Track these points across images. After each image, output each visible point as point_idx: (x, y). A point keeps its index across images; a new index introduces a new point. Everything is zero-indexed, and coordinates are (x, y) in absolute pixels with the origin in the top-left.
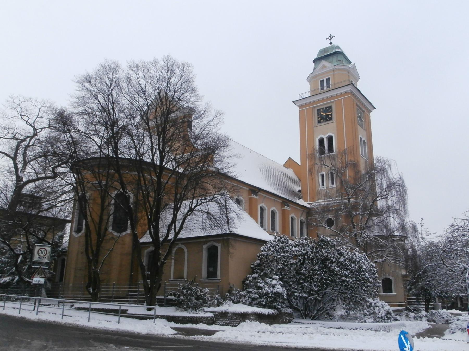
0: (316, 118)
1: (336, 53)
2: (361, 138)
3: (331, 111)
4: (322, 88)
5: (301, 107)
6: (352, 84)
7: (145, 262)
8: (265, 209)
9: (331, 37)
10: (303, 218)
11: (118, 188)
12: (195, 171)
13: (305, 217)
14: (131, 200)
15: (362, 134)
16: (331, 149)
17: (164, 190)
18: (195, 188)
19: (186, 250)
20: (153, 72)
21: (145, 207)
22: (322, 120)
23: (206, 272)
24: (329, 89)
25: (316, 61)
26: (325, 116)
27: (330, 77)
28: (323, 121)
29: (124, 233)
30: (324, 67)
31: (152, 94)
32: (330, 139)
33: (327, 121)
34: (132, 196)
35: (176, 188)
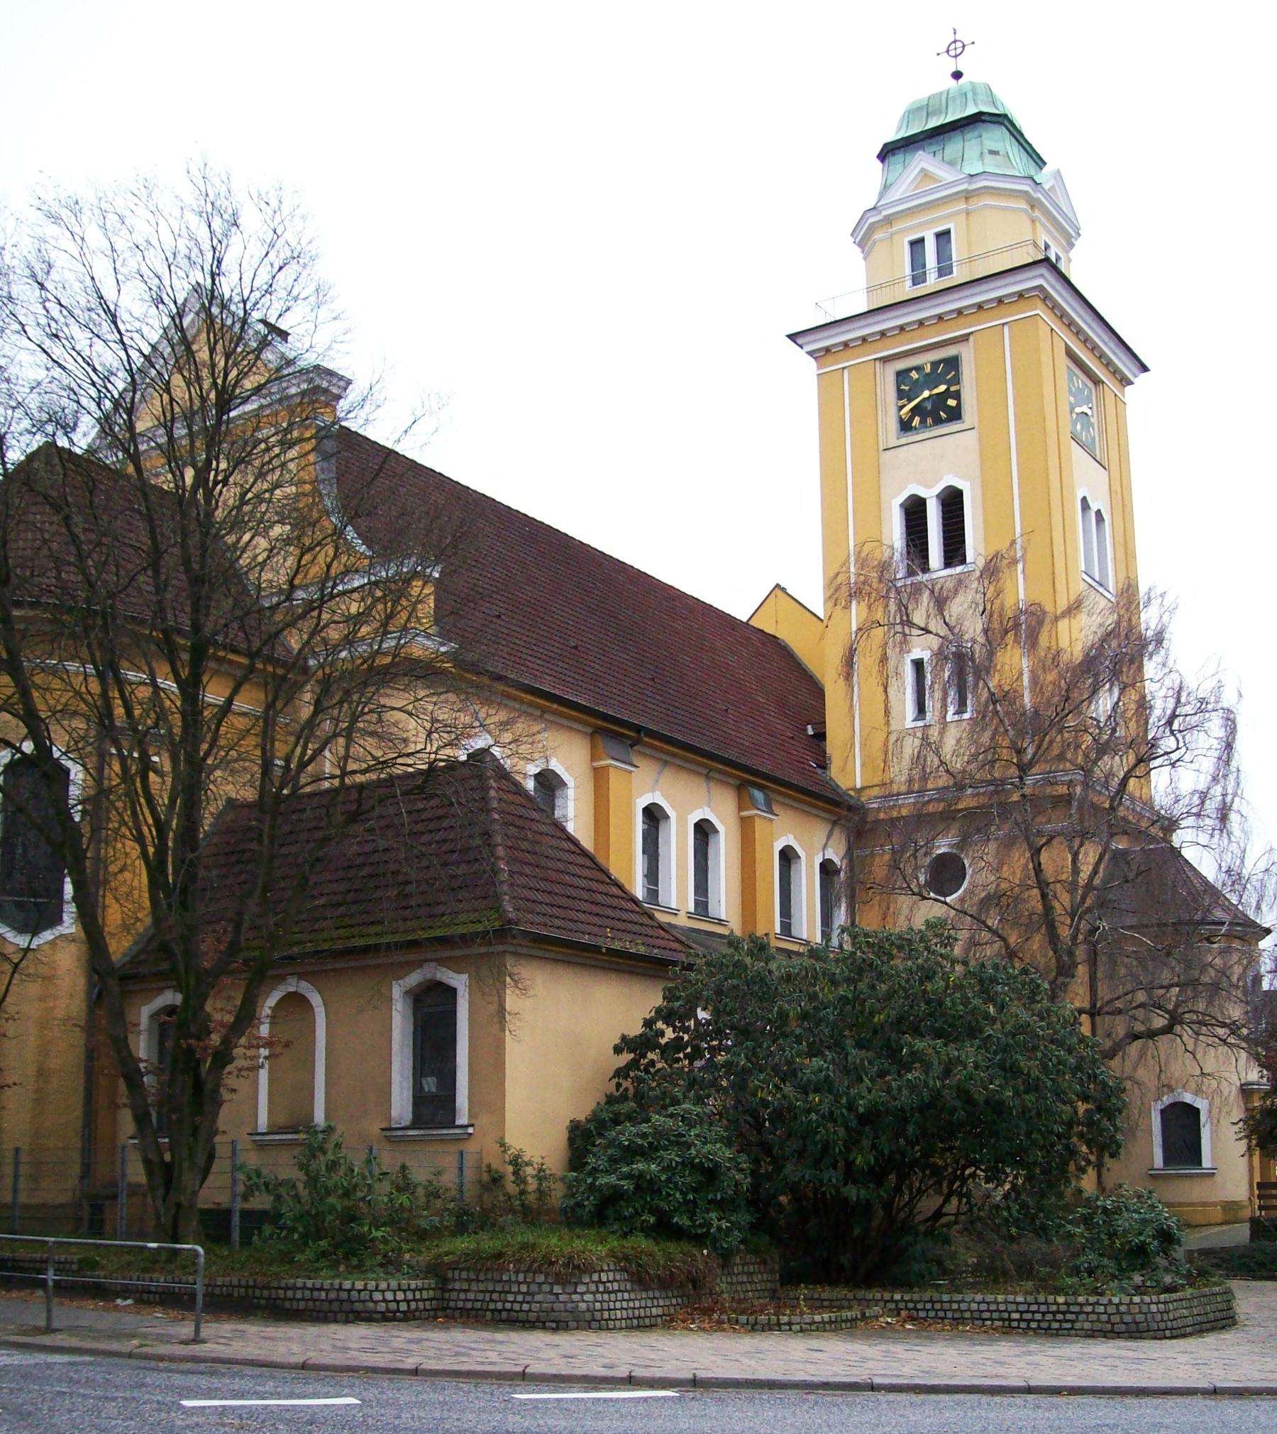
0: (892, 410)
1: (977, 119)
2: (1084, 500)
3: (957, 380)
4: (918, 279)
5: (821, 355)
6: (1047, 260)
7: (143, 1047)
8: (667, 817)
9: (956, 48)
10: (835, 854)
11: (10, 737)
12: (343, 654)
13: (842, 849)
14: (74, 791)
15: (1087, 480)
16: (954, 551)
17: (213, 744)
18: (349, 735)
19: (316, 1000)
20: (143, 230)
21: (134, 814)
22: (917, 419)
23: (408, 1094)
24: (922, 290)
25: (887, 152)
26: (932, 401)
27: (951, 226)
28: (923, 422)
29: (48, 936)
30: (925, 174)
31: (148, 327)
32: (952, 502)
33: (938, 421)
34: (77, 773)
35: (267, 738)
